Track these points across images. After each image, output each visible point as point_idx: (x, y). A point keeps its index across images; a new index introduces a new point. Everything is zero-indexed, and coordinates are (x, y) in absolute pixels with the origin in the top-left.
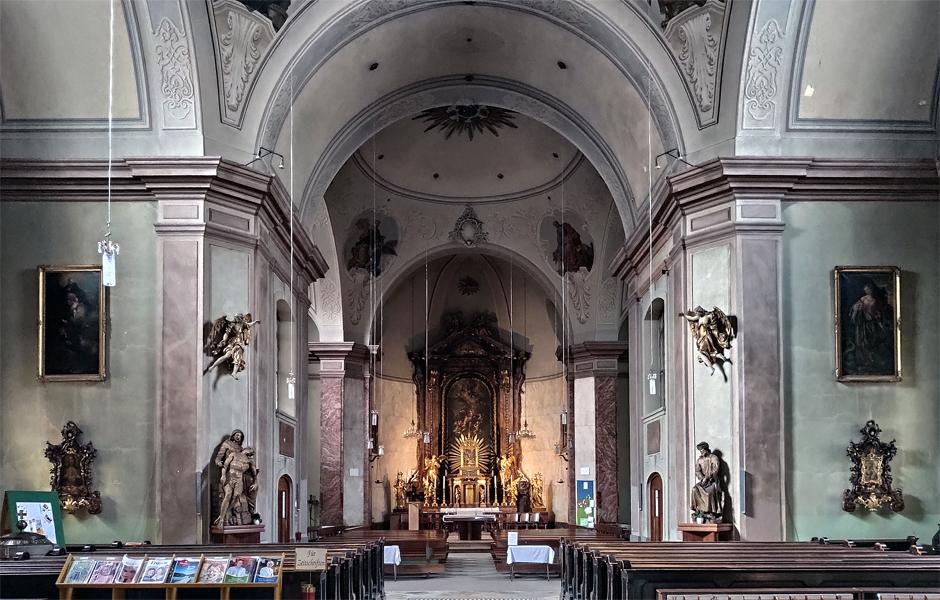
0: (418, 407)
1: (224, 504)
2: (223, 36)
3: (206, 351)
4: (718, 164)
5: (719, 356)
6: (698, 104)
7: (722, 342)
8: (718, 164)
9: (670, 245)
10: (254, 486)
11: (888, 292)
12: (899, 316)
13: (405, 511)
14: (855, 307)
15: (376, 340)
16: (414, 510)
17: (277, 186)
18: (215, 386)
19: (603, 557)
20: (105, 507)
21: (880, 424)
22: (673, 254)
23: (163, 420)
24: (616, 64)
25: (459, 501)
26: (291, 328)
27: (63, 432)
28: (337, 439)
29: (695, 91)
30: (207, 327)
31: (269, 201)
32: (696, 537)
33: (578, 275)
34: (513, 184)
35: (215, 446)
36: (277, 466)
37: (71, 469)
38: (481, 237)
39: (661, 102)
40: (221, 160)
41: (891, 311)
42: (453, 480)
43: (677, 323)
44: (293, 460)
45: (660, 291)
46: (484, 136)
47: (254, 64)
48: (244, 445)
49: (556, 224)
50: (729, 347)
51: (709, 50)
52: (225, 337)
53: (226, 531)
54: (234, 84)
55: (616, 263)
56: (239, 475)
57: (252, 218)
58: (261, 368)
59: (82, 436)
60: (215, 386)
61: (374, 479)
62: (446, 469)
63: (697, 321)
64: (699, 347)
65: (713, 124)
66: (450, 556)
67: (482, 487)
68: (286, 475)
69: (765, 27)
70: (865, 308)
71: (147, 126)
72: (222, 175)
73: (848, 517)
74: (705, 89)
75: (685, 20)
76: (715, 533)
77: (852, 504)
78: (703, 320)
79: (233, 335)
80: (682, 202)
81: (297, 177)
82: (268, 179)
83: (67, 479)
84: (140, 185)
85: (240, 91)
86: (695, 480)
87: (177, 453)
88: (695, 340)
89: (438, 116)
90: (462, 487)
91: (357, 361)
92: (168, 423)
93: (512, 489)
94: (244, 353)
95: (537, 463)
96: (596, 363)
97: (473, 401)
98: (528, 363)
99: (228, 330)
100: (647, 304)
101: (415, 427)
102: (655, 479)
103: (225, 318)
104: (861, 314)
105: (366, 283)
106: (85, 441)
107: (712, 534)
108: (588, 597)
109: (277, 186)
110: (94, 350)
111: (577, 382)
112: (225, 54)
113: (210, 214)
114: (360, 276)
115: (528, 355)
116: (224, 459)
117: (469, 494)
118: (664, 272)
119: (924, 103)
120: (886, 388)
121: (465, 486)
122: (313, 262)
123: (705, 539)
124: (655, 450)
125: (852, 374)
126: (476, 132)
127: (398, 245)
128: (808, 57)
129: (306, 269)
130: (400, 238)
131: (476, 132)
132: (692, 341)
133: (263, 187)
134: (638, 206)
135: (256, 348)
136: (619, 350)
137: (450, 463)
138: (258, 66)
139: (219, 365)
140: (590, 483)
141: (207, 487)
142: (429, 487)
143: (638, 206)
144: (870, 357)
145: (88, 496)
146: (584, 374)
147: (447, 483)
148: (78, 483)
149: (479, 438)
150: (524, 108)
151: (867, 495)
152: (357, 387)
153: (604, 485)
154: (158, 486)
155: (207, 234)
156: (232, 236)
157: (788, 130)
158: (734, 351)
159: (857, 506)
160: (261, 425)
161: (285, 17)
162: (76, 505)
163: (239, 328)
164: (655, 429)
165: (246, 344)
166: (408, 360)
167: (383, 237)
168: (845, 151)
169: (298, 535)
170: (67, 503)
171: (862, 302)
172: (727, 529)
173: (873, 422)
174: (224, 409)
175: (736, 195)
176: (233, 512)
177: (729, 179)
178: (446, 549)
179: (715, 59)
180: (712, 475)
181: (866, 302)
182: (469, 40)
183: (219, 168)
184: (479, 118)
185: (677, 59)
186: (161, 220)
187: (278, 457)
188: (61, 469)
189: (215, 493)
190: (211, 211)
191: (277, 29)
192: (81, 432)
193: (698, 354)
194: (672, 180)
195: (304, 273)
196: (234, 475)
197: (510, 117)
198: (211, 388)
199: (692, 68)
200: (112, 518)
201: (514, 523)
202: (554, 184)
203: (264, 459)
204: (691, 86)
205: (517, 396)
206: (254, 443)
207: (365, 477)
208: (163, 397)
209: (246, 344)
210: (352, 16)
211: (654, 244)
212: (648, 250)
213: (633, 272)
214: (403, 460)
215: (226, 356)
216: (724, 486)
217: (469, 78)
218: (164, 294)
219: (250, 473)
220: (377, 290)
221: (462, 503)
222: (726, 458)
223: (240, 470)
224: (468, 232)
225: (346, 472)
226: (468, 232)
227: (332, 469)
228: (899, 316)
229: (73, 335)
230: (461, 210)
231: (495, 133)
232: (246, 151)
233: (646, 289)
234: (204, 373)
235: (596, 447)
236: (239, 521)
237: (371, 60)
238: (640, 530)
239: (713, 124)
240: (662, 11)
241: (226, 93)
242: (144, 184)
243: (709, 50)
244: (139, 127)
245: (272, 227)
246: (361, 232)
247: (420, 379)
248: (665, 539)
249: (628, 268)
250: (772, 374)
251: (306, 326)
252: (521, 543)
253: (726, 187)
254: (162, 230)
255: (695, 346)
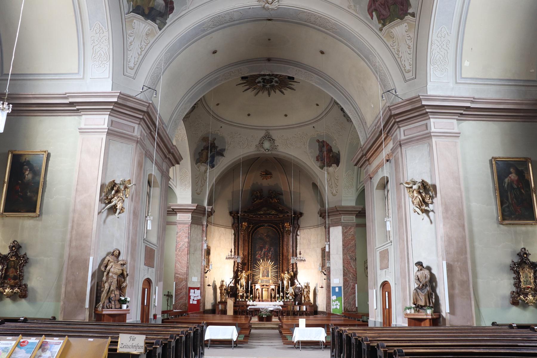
0: (235, 242)
1: (104, 295)
2: (129, 32)
3: (100, 200)
4: (418, 99)
5: (426, 208)
6: (403, 69)
7: (427, 200)
8: (418, 99)
9: (391, 145)
10: (124, 284)
11: (526, 173)
12: (533, 186)
13: (225, 303)
14: (506, 180)
15: (209, 204)
16: (230, 302)
17: (153, 108)
18: (105, 221)
19: (359, 337)
20: (30, 294)
21: (529, 249)
22: (393, 150)
23: (71, 241)
24: (353, 50)
25: (259, 298)
26: (156, 192)
27: (10, 247)
28: (184, 260)
29: (401, 62)
30: (102, 186)
31: (147, 116)
32: (416, 322)
33: (331, 169)
34: (292, 120)
35: (101, 258)
36: (141, 272)
37: (11, 270)
38: (274, 147)
39: (381, 69)
40: (120, 93)
41: (528, 183)
42: (255, 286)
43: (398, 190)
44: (154, 269)
45: (386, 172)
46: (276, 95)
47: (146, 46)
48: (121, 258)
49: (318, 141)
50: (432, 203)
51: (408, 42)
52: (113, 192)
53: (104, 312)
54: (133, 55)
55: (356, 158)
56: (115, 277)
57: (136, 126)
58: (134, 212)
59: (21, 250)
60: (105, 221)
61: (207, 284)
62: (252, 280)
63: (412, 187)
64: (413, 203)
65: (413, 79)
66: (253, 331)
67: (273, 289)
68: (148, 279)
69: (440, 29)
70: (512, 182)
71: (82, 77)
72: (121, 101)
73: (514, 309)
74: (406, 61)
75: (393, 27)
76: (430, 319)
77: (516, 300)
78: (415, 187)
79: (117, 191)
80: (397, 120)
81: (168, 107)
82: (148, 104)
83: (8, 276)
84: (74, 107)
85: (136, 59)
86: (414, 285)
87: (78, 263)
88: (411, 199)
89: (249, 81)
90: (260, 290)
91: (201, 216)
92: (74, 244)
93: (291, 290)
94: (124, 202)
95: (308, 275)
96: (344, 218)
97: (268, 240)
98: (301, 219)
99: (115, 189)
100: (376, 180)
101: (233, 253)
102: (385, 285)
103: (114, 181)
104: (510, 184)
105: (206, 172)
106: (22, 252)
107: (428, 320)
108: (340, 356)
109: (153, 108)
110: (35, 198)
111: (331, 229)
112: (130, 41)
113: (112, 123)
114: (203, 168)
115: (301, 214)
116: (106, 267)
117: (265, 293)
118: (387, 161)
119: (533, 71)
120: (530, 228)
121: (262, 289)
122: (173, 154)
123: (423, 324)
124: (385, 266)
125: (508, 220)
126: (272, 92)
127: (226, 151)
128: (460, 52)
129: (169, 158)
130: (227, 147)
131: (272, 92)
132: (409, 200)
133: (145, 109)
134: (369, 126)
135: (132, 200)
136: (356, 211)
137: (254, 276)
138: (147, 47)
139: (109, 209)
140: (340, 288)
141: (94, 283)
142: (241, 291)
143: (369, 126)
144: (519, 210)
145: (20, 287)
146: (336, 224)
147: (251, 287)
148: (15, 278)
149: (272, 261)
150: (299, 75)
151: (526, 295)
152: (198, 230)
153: (348, 289)
154: (64, 282)
155: (108, 134)
156: (123, 135)
157: (456, 83)
158: (437, 205)
159: (520, 301)
160: (133, 245)
161: (165, 24)
162: (12, 292)
163: (122, 188)
164: (385, 255)
165: (126, 197)
166: (229, 216)
167: (217, 147)
168: (491, 95)
169: (155, 316)
170: (6, 291)
171: (510, 177)
172: (438, 316)
173: (525, 249)
174: (110, 236)
175: (430, 116)
176: (110, 300)
177: (426, 107)
178: (250, 328)
179: (412, 46)
180: (426, 282)
181: (512, 177)
182: (269, 40)
183: (119, 97)
184: (273, 85)
185: (390, 46)
186: (83, 126)
187: (142, 266)
188: (6, 269)
189: (99, 288)
190: (112, 121)
191: (160, 29)
192: (21, 247)
193: (412, 207)
194: (391, 108)
195: (167, 160)
196: (112, 276)
197: (292, 85)
198: (102, 222)
199: (398, 51)
200: (33, 301)
201: (303, 311)
202: (317, 120)
203: (133, 268)
204: (399, 60)
205: (295, 237)
206: (127, 257)
207: (201, 282)
208: (72, 227)
209: (126, 197)
210: (203, 24)
211: (385, 139)
212: (382, 143)
213: (367, 163)
214: (222, 270)
215: (112, 204)
216: (434, 289)
217: (269, 60)
218: (80, 166)
219: (122, 276)
220: (212, 175)
221: (260, 299)
222: (434, 271)
223: (116, 274)
224: (267, 145)
225: (190, 279)
226: (267, 145)
227: (181, 277)
228: (533, 186)
229: (24, 189)
230: (262, 134)
231: (283, 93)
232: (136, 89)
233: (376, 172)
234: (99, 213)
235: (344, 267)
236: (113, 306)
237: (213, 49)
238: (375, 318)
239: (413, 79)
240: (379, 22)
241: (128, 59)
242: (75, 106)
243: (408, 42)
244: (77, 77)
245: (148, 132)
246: (205, 144)
247: (236, 227)
248: (394, 323)
249: (363, 159)
250: (460, 219)
251: (168, 192)
252: (307, 326)
253: (424, 111)
254: (82, 131)
255: (411, 203)
